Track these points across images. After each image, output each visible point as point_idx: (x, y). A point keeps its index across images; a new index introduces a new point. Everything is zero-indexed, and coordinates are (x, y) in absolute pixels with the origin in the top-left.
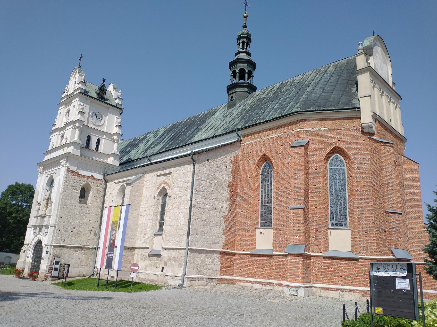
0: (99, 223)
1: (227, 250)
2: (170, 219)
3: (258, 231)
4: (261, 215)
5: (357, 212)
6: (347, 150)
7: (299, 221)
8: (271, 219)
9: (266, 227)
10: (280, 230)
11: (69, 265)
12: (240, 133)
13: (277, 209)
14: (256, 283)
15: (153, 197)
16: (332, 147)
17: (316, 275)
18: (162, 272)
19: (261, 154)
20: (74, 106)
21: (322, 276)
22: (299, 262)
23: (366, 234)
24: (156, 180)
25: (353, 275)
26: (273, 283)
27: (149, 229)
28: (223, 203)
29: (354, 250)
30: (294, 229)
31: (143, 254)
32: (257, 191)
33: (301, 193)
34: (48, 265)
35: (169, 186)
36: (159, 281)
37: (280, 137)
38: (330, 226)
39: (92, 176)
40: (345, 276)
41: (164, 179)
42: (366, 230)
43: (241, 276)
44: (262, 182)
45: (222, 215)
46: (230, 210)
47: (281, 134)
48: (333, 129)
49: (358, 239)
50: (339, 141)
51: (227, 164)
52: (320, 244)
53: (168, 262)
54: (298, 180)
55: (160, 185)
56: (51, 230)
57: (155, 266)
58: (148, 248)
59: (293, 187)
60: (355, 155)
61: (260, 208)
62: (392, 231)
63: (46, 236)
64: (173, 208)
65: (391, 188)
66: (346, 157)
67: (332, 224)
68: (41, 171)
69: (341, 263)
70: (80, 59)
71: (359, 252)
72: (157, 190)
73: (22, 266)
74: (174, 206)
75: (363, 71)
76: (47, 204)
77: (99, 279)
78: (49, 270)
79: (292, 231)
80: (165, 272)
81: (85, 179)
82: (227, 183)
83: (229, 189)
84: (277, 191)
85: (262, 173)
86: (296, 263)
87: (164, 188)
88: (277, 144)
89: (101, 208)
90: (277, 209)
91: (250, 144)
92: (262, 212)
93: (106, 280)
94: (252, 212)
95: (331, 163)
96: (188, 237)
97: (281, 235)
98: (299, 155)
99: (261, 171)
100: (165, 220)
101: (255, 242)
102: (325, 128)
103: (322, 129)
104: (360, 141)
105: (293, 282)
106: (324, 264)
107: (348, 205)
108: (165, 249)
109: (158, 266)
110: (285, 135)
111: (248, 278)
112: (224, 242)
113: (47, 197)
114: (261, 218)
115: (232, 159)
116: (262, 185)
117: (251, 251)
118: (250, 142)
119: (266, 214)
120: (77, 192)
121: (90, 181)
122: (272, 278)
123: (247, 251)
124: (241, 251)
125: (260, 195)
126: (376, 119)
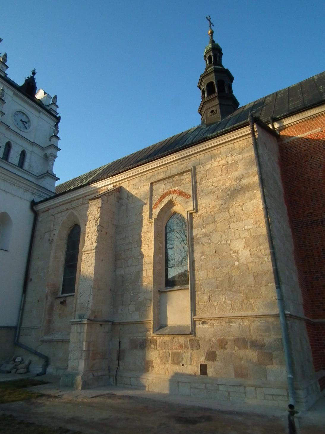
2: (203, 257)
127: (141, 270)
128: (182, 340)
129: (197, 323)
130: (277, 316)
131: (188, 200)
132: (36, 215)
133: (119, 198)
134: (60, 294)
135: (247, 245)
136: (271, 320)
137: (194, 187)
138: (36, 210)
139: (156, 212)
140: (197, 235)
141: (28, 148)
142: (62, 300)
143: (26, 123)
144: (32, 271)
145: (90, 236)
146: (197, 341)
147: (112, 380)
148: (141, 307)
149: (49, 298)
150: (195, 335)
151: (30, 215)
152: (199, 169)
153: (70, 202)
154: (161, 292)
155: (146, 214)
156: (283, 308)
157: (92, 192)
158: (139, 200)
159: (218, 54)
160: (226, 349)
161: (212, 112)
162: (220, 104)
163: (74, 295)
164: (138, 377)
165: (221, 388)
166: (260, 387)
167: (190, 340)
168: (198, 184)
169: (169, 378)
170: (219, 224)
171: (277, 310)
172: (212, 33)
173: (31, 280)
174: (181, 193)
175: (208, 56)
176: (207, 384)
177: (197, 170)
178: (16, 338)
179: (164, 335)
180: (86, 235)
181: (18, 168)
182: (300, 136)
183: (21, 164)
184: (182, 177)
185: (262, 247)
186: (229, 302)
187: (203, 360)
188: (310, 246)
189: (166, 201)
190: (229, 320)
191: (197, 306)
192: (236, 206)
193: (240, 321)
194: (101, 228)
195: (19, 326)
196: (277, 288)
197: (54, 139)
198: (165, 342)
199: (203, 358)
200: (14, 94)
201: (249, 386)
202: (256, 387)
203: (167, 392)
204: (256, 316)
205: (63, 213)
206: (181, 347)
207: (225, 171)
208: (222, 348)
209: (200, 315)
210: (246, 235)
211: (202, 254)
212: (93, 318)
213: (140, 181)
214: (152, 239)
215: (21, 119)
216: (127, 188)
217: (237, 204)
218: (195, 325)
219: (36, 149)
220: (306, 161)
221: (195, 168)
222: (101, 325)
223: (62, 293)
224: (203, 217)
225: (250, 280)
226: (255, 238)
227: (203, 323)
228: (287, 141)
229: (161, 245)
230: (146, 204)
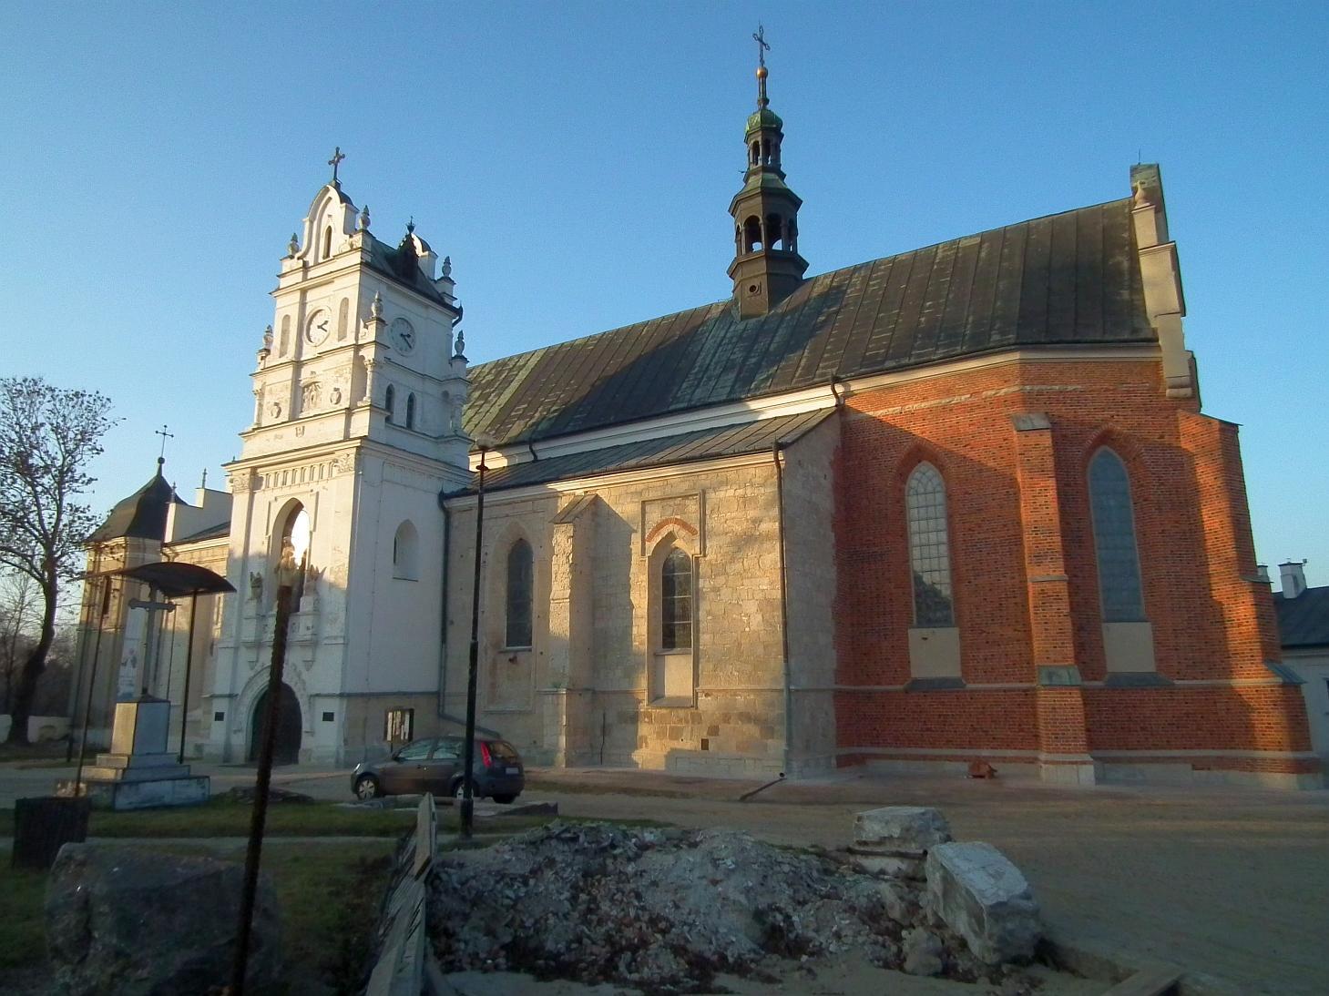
2: (710, 618)
3: (914, 634)
37: (962, 406)
43: (878, 744)
47: (963, 398)
70: (335, 163)
127: (631, 626)
128: (682, 713)
129: (699, 694)
130: (782, 691)
131: (694, 537)
132: (447, 514)
133: (595, 514)
134: (504, 646)
135: (760, 609)
136: (775, 694)
137: (703, 522)
138: (446, 506)
139: (651, 546)
140: (704, 587)
141: (415, 385)
142: (511, 656)
143: (409, 336)
144: (451, 609)
145: (559, 577)
146: (699, 715)
147: (597, 758)
148: (630, 673)
149: (489, 652)
150: (697, 708)
151: (438, 516)
152: (713, 497)
153: (510, 503)
154: (656, 655)
155: (636, 546)
156: (788, 683)
157: (548, 495)
158: (625, 524)
159: (774, 140)
160: (729, 723)
161: (752, 289)
162: (769, 274)
163: (530, 650)
164: (629, 755)
165: (722, 762)
166: (760, 760)
167: (691, 713)
168: (708, 517)
169: (665, 753)
170: (730, 577)
171: (782, 686)
172: (764, 75)
173: (452, 623)
174: (685, 525)
175: (752, 142)
176: (533, 462)
177: (707, 496)
178: (441, 708)
179: (661, 708)
180: (553, 576)
181: (407, 431)
182: (871, 413)
183: (410, 425)
184: (687, 502)
185: (775, 613)
186: (736, 674)
187: (704, 735)
188: (864, 589)
189: (664, 532)
190: (735, 693)
191: (700, 676)
192: (751, 554)
193: (746, 694)
194: (574, 567)
195: (442, 690)
196: (785, 661)
198: (663, 715)
199: (705, 733)
200: (389, 287)
201: (748, 758)
202: (755, 759)
203: (662, 768)
204: (762, 690)
205: (499, 520)
206: (680, 721)
207: (742, 506)
208: (725, 722)
209: (703, 686)
210: (759, 596)
211: (709, 613)
212: (571, 687)
213: (627, 493)
214: (645, 584)
215: (400, 332)
216: (606, 500)
217: (754, 555)
218: (697, 697)
220: (874, 459)
221: (704, 492)
222: (580, 695)
223: (507, 646)
224: (712, 565)
225: (760, 650)
226: (769, 601)
227: (707, 695)
228: (852, 417)
229: (656, 592)
230: (636, 532)
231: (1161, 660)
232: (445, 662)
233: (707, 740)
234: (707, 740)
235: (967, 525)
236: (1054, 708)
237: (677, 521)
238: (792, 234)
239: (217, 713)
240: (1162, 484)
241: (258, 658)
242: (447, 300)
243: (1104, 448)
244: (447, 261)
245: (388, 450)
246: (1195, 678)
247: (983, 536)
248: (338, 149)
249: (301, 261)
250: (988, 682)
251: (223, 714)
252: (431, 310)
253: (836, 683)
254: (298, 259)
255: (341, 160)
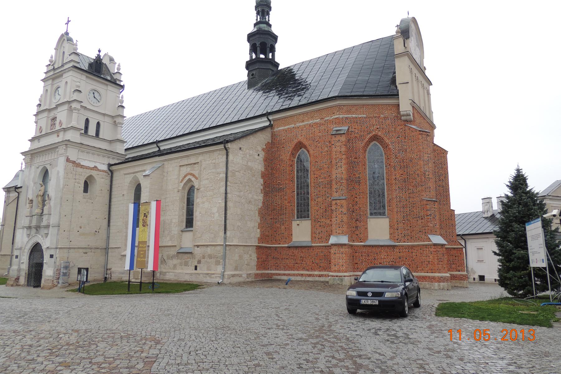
0: (107, 220)
1: (352, 242)
2: (201, 215)
3: (294, 224)
4: (297, 206)
5: (395, 201)
6: (385, 139)
7: (342, 211)
8: (308, 211)
9: (303, 219)
10: (319, 222)
11: (87, 269)
12: (271, 118)
13: (315, 200)
14: (294, 275)
15: (176, 190)
16: (371, 135)
17: (357, 264)
18: (196, 271)
19: (296, 141)
20: (66, 82)
21: (362, 264)
22: (343, 252)
23: (403, 222)
24: (180, 171)
25: (391, 261)
26: (314, 275)
27: (175, 226)
28: (256, 196)
29: (313, 238)
30: (337, 220)
31: (169, 252)
32: (292, 181)
33: (343, 183)
34: (55, 270)
35: (197, 178)
36: (194, 279)
37: (316, 124)
38: (369, 215)
39: (95, 167)
40: (384, 263)
41: (189, 170)
42: (404, 218)
43: (278, 270)
44: (297, 171)
45: (256, 208)
46: (264, 203)
47: (317, 120)
48: (372, 116)
49: (396, 226)
50: (378, 128)
51: (259, 152)
52: (360, 234)
53: (203, 260)
54: (340, 170)
55: (185, 176)
56: (52, 231)
57: (186, 264)
58: (175, 246)
59: (334, 177)
60: (393, 143)
61: (296, 199)
62: (429, 219)
63: (47, 238)
64: (203, 203)
65: (427, 176)
66: (385, 146)
67: (371, 214)
68: (29, 161)
69: (380, 251)
70: (67, 24)
71: (397, 240)
72: (181, 182)
73: (16, 274)
74: (205, 199)
75: (401, 55)
76: (44, 201)
77: (141, 282)
78: (57, 276)
79: (335, 222)
80: (198, 271)
81: (88, 171)
82: (260, 173)
83: (262, 181)
84: (315, 181)
85: (297, 162)
86: (340, 253)
87: (190, 180)
88: (313, 130)
89: (108, 204)
90: (315, 200)
91: (283, 130)
92: (298, 203)
93: (151, 283)
94: (288, 204)
95: (369, 152)
96: (225, 233)
97: (320, 226)
98: (340, 144)
99: (296, 160)
100: (194, 216)
101: (292, 235)
102: (364, 114)
103: (360, 116)
104: (398, 129)
105: (337, 272)
106: (365, 252)
107: (386, 194)
108: (198, 246)
109: (190, 264)
110: (322, 121)
111: (285, 271)
112: (259, 236)
113: (41, 193)
114: (297, 210)
115: (264, 147)
116: (297, 175)
117: (288, 244)
118: (283, 127)
119: (302, 206)
120: (80, 186)
121: (94, 173)
122: (312, 269)
123: (283, 244)
124: (276, 244)
125: (296, 185)
126: (413, 107)
141: (100, 118)
188: (276, 204)
197: (120, 109)
200: (87, 77)
219: (107, 119)
231: (391, 234)
232: (109, 235)
233: (197, 266)
234: (197, 266)
235: (316, 176)
236: (335, 253)
237: (191, 174)
238: (273, 50)
239: (16, 256)
240: (397, 158)
241: (30, 233)
242: (118, 82)
243: (374, 142)
244: (119, 65)
245: (80, 146)
246: (404, 242)
247: (320, 180)
248: (68, 18)
249: (53, 66)
250: (320, 243)
251: (53, 255)
252: (109, 86)
253: (259, 243)
254: (52, 66)
255: (69, 23)
